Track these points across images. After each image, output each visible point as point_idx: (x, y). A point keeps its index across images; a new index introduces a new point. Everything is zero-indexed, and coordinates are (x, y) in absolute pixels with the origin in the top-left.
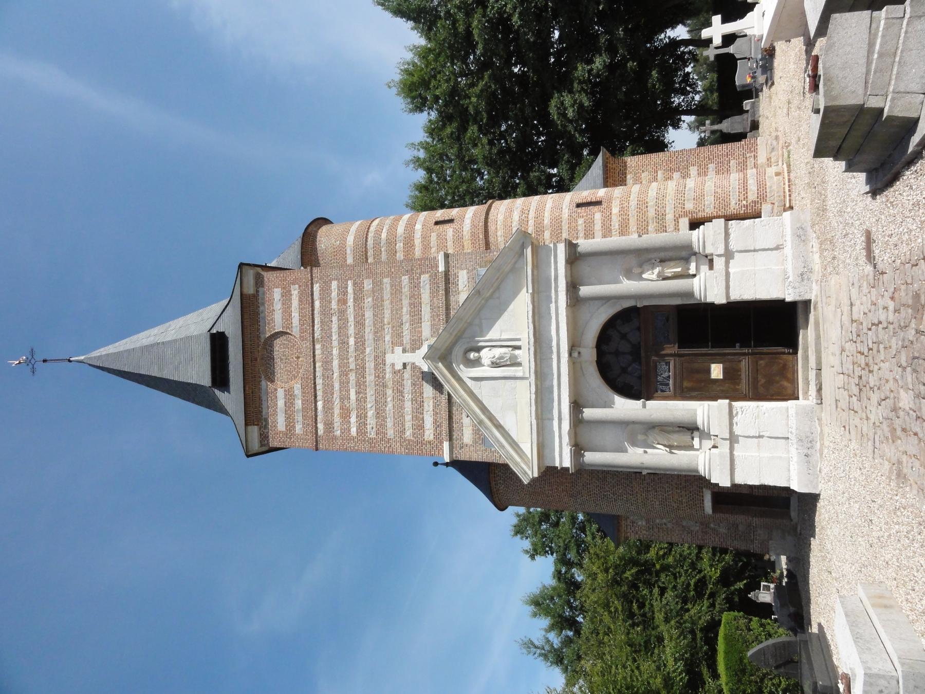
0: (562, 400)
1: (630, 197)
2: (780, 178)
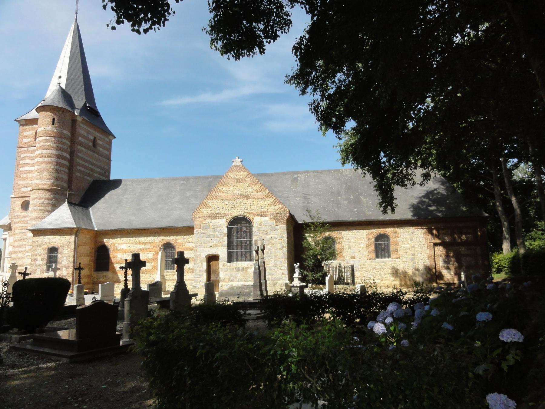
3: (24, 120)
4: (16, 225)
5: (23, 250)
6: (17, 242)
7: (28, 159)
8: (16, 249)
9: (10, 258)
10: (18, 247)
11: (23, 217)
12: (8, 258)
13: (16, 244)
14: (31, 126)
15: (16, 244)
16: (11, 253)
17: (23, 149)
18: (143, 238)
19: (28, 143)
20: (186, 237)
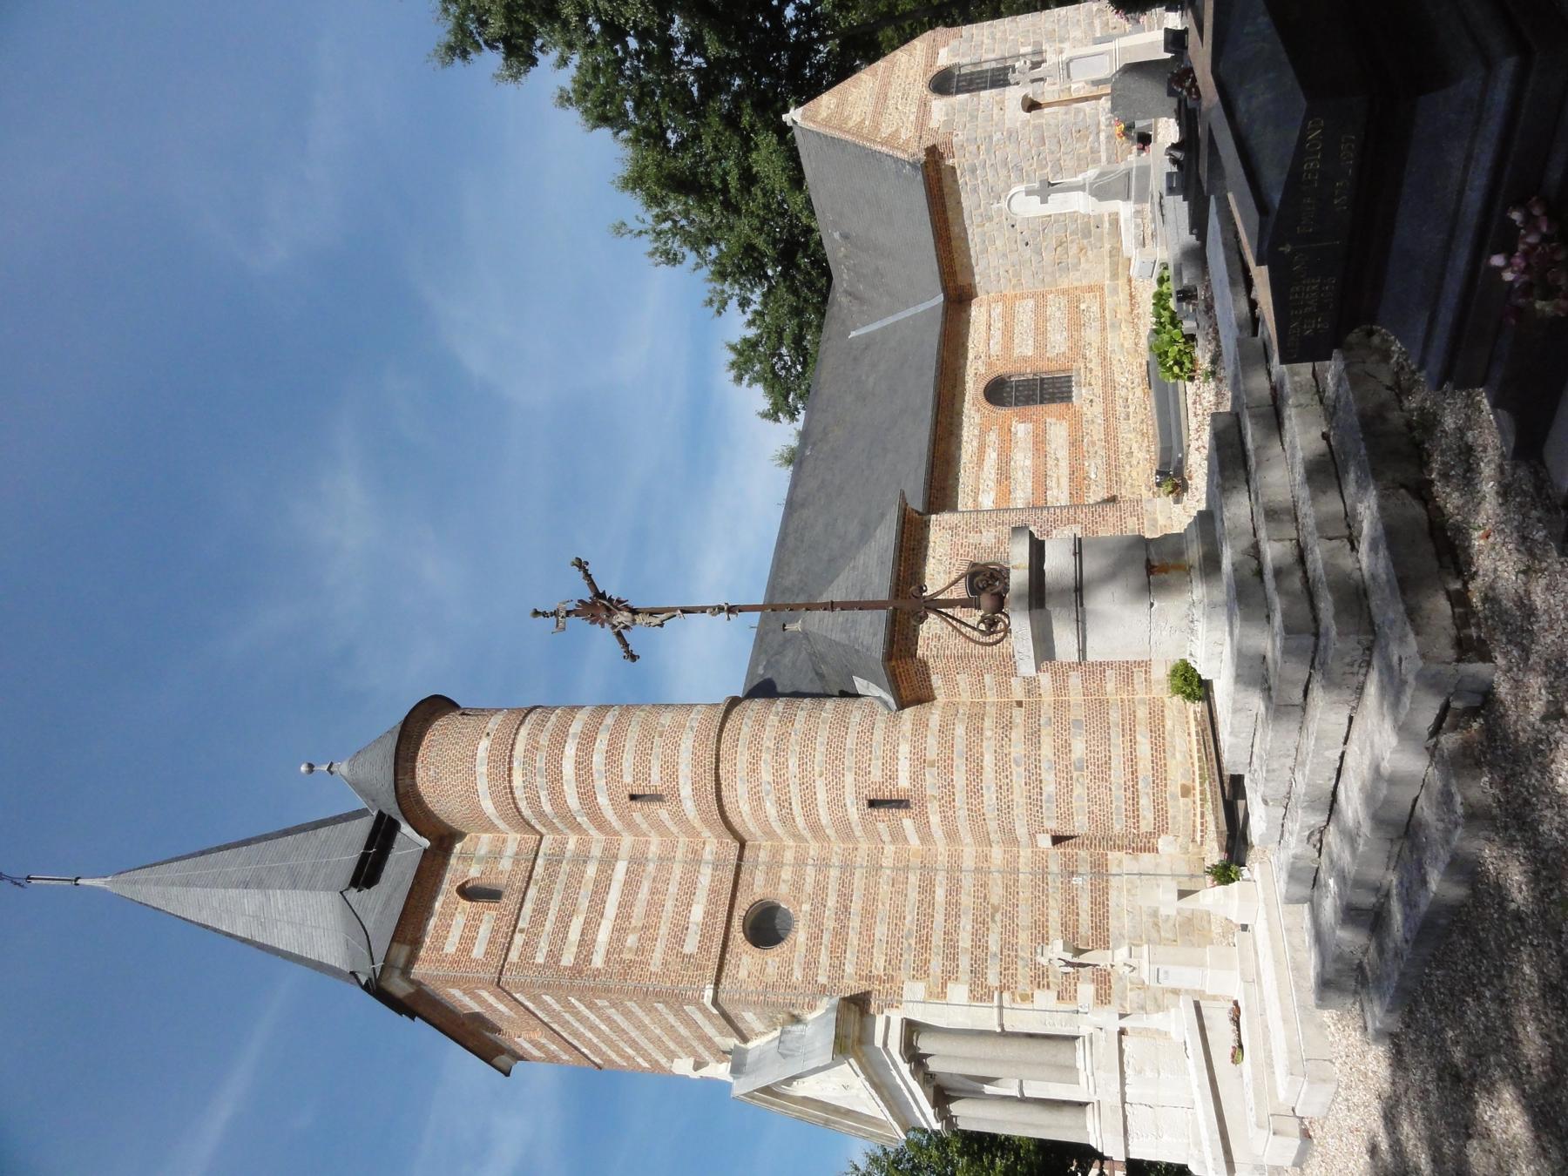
0: (968, 1025)
1: (954, 800)
2: (1189, 800)
3: (393, 939)
4: (849, 969)
5: (969, 927)
6: (927, 961)
7: (567, 926)
8: (964, 962)
9: (1006, 995)
10: (951, 953)
11: (815, 938)
12: (1006, 1004)
13: (936, 965)
14: (432, 922)
15: (936, 965)
16: (980, 993)
17: (514, 956)
18: (963, 451)
19: (495, 931)
20: (971, 355)
